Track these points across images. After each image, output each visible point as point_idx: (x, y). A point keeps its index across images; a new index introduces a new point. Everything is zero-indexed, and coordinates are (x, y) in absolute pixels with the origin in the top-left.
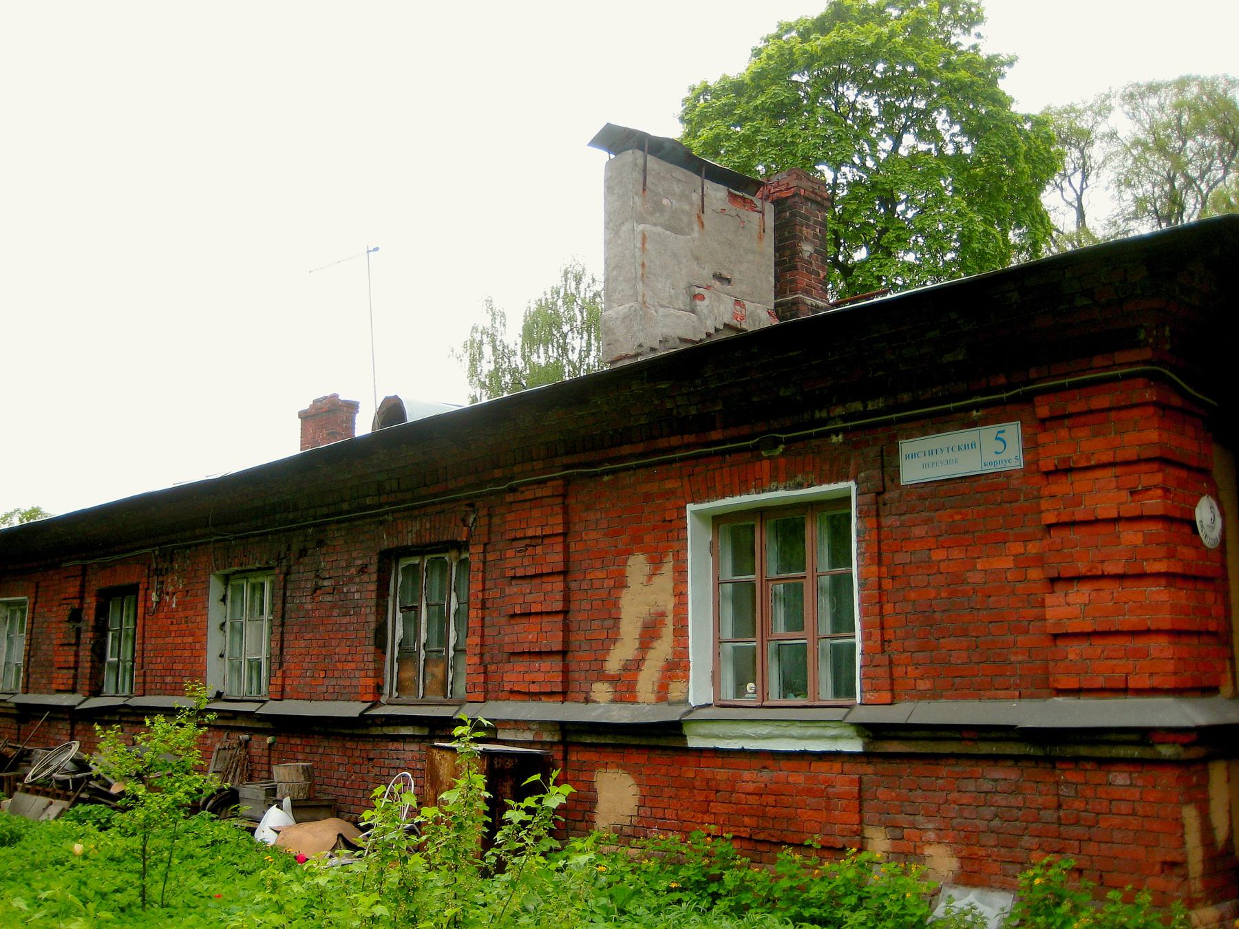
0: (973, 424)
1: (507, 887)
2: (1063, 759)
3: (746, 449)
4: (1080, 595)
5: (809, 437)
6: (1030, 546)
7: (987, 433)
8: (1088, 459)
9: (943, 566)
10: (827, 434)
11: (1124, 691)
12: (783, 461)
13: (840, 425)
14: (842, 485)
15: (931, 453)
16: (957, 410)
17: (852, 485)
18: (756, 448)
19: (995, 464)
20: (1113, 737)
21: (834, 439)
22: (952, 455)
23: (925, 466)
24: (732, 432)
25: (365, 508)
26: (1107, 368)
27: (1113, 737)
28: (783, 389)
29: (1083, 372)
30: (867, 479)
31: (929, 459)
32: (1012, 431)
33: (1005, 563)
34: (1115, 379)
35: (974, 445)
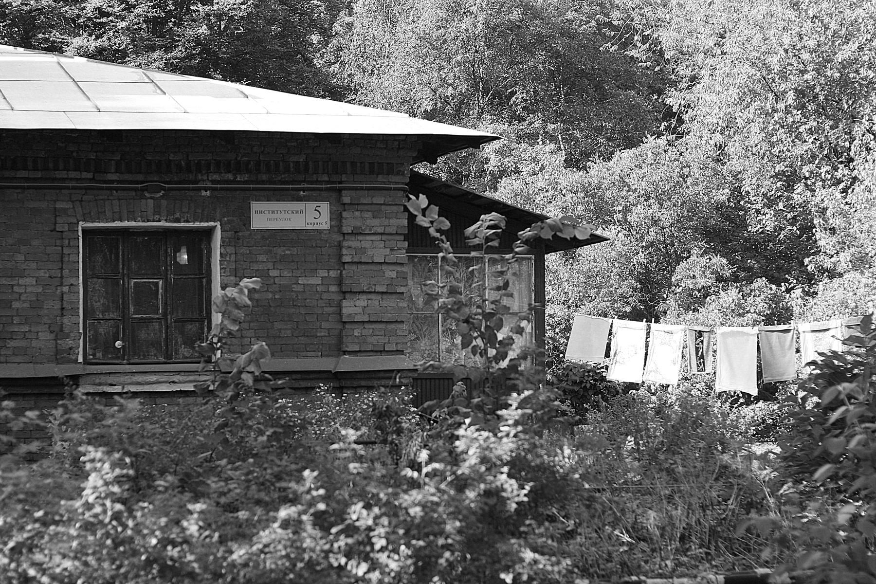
0: (300, 199)
1: (735, 176)
2: (374, 378)
3: (136, 190)
4: (362, 301)
5: (288, 189)
6: (331, 272)
7: (310, 206)
8: (370, 230)
9: (277, 280)
10: (200, 189)
11: (382, 352)
12: (164, 202)
13: (209, 185)
14: (212, 224)
15: (273, 212)
16: (293, 189)
17: (218, 224)
18: (143, 190)
19: (314, 224)
20: (382, 375)
21: (203, 193)
22: (287, 216)
23: (268, 219)
24: (127, 177)
25: (54, 180)
26: (384, 183)
27: (382, 375)
28: (172, 155)
29: (371, 182)
30: (229, 222)
31: (271, 216)
32: (325, 207)
33: (317, 281)
34: (389, 189)
35: (301, 212)
